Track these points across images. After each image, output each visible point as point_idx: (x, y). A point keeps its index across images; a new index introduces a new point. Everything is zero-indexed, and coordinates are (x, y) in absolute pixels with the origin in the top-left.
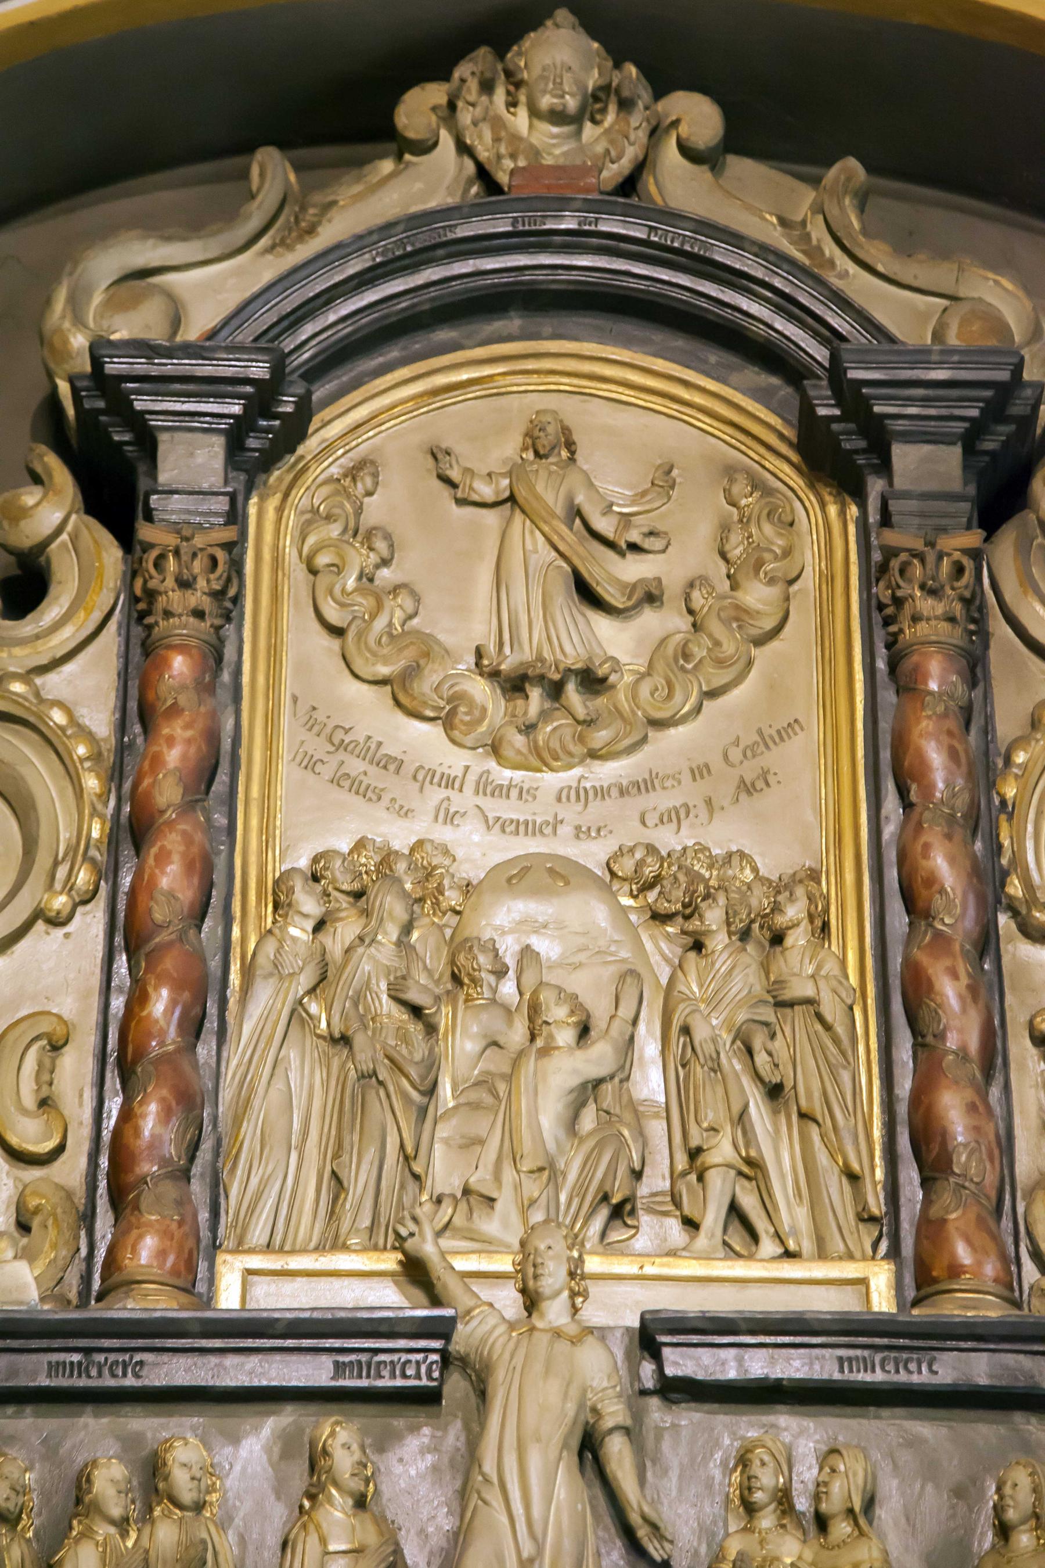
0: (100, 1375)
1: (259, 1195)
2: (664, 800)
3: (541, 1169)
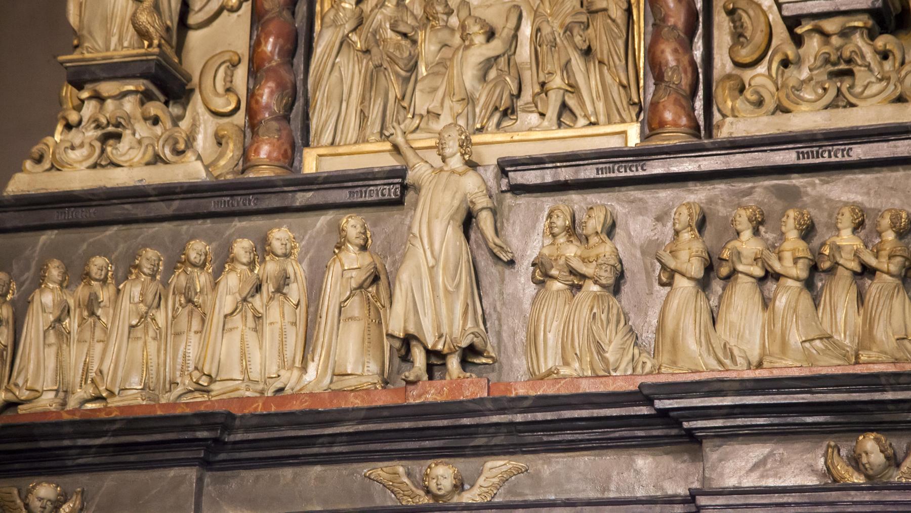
1: (326, 121)
3: (463, 99)
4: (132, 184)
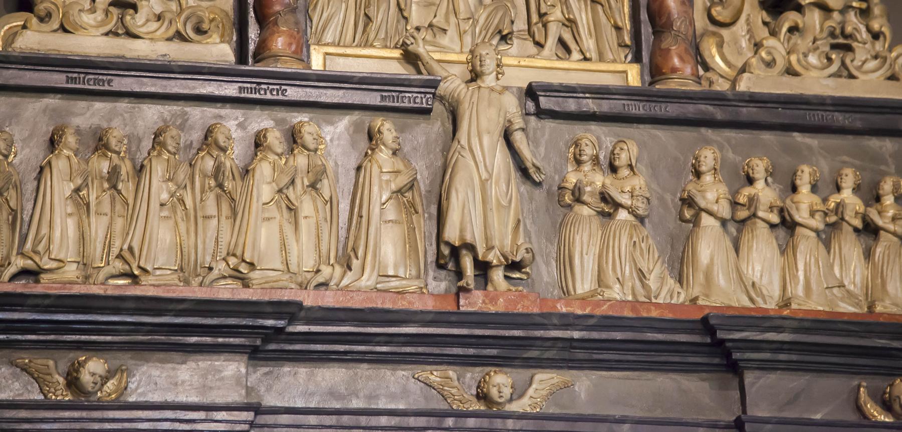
0: (278, 94)
3: (469, 19)
4: (154, 57)
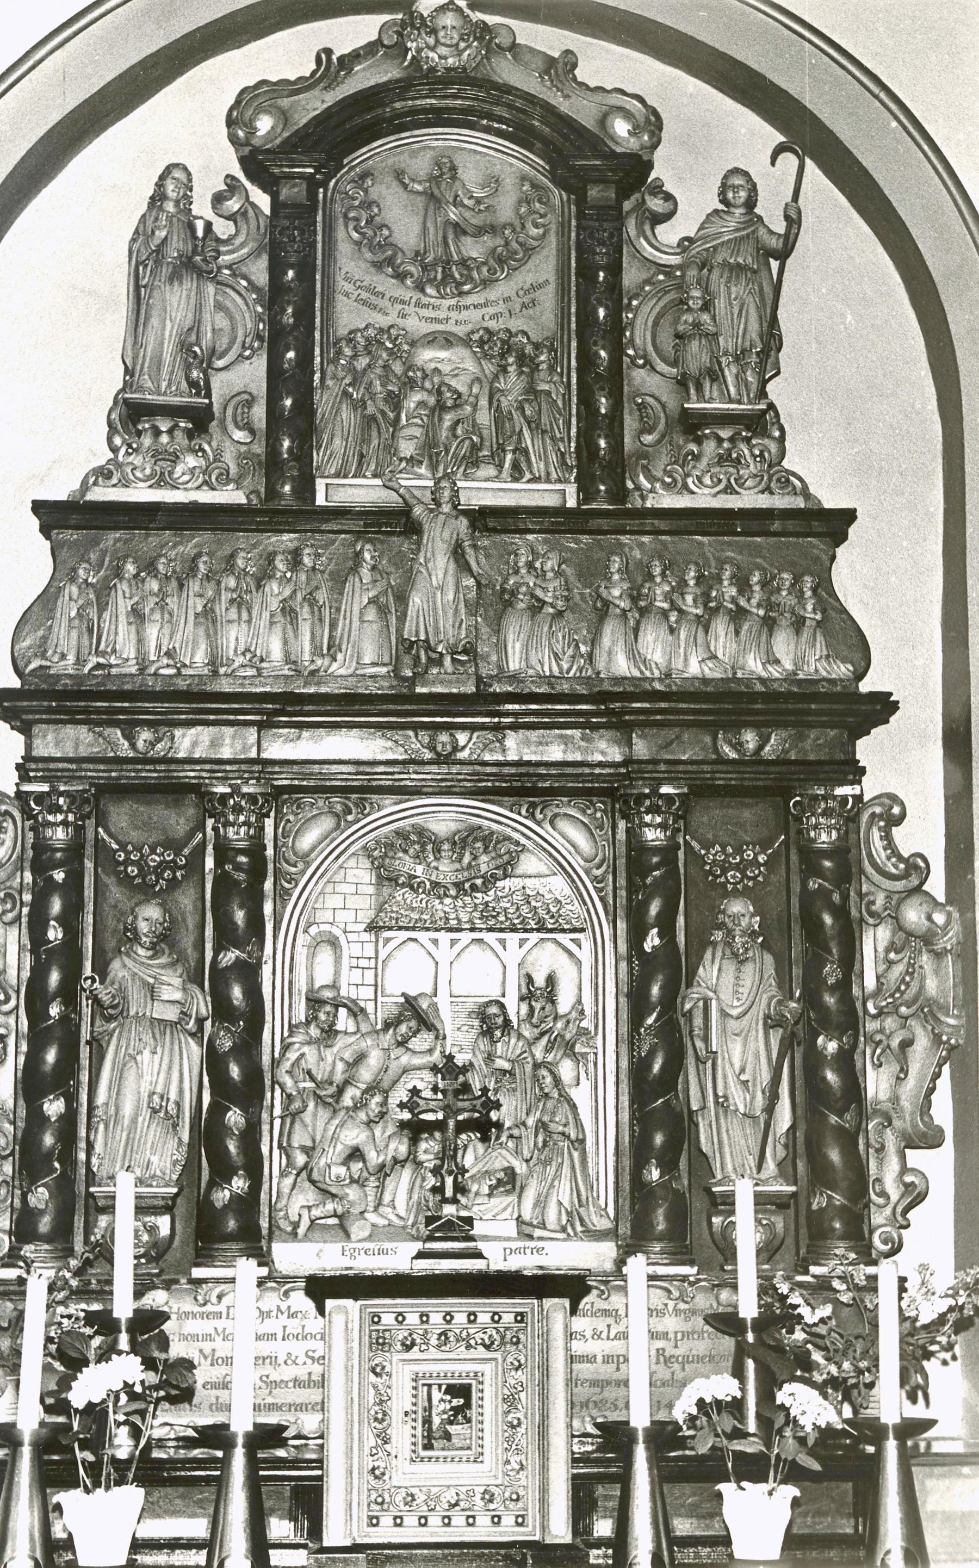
2: (491, 310)
